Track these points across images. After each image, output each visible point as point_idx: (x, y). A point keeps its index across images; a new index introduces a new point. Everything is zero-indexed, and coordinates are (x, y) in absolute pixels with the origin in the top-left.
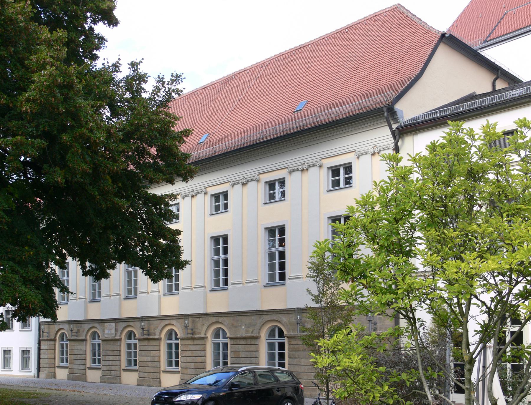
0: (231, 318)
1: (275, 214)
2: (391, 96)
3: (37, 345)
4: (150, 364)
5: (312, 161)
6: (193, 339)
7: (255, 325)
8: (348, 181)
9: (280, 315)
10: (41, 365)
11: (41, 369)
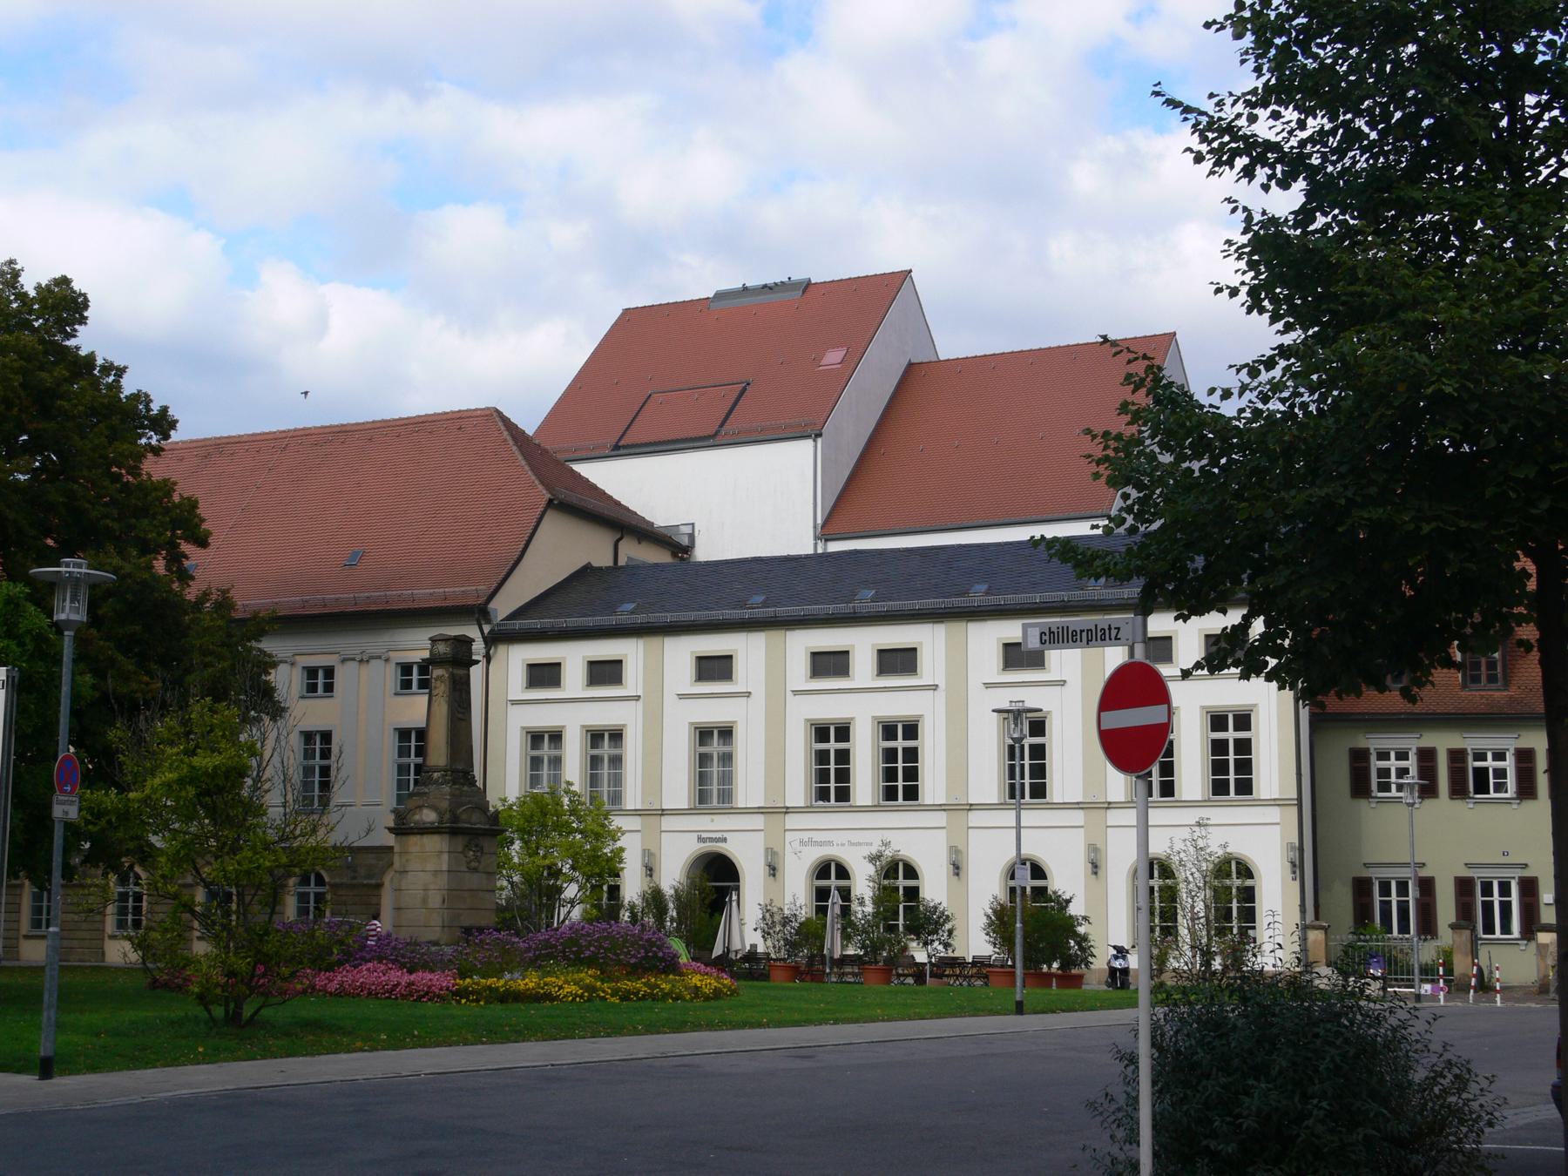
2: (485, 588)
5: (377, 652)
8: (329, 688)
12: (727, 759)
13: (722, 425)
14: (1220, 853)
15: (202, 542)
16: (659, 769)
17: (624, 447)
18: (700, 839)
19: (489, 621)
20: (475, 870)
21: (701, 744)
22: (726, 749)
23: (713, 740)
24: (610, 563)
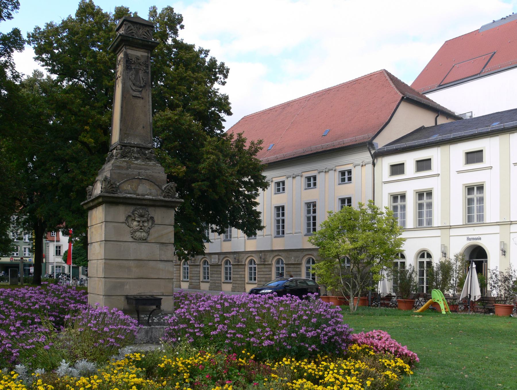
2: (372, 135)
5: (331, 167)
12: (481, 200)
13: (484, 68)
14: (436, 301)
15: (229, 113)
16: (449, 206)
17: (443, 85)
18: (468, 239)
19: (374, 149)
20: (144, 240)
21: (469, 194)
22: (481, 195)
23: (475, 190)
24: (434, 124)
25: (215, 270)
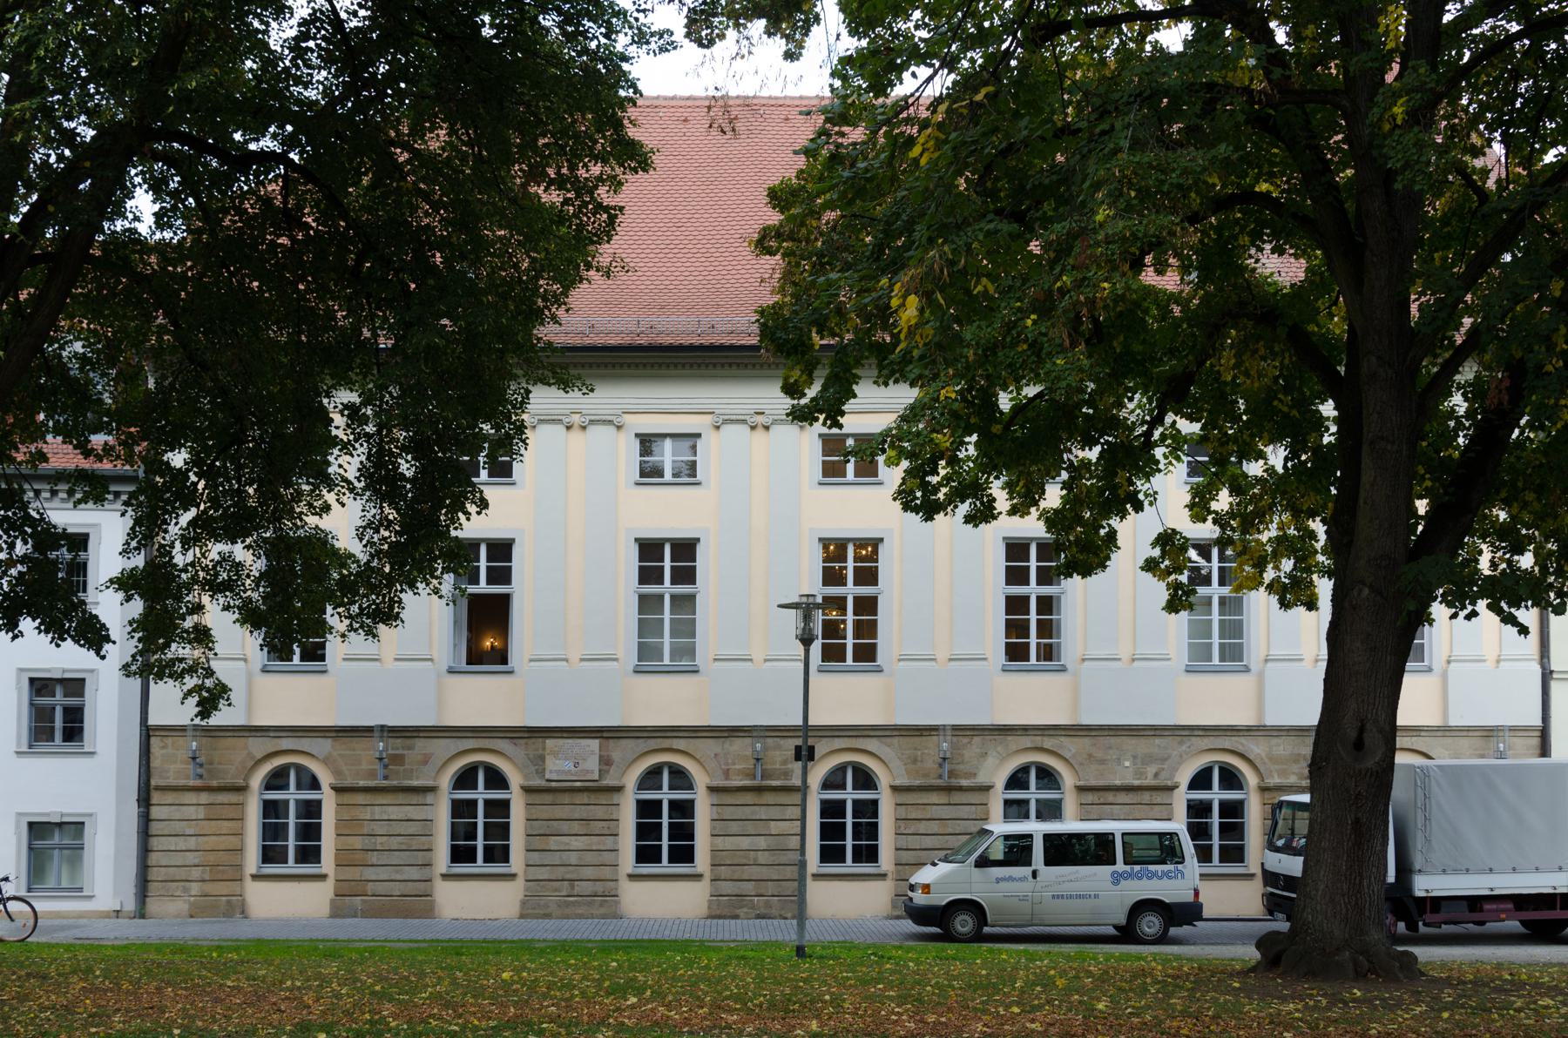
0: (1086, 740)
1: (666, 511)
3: (133, 810)
4: (763, 858)
6: (949, 789)
7: (1164, 760)
9: (1243, 740)
10: (154, 874)
11: (152, 887)
25: (579, 812)
